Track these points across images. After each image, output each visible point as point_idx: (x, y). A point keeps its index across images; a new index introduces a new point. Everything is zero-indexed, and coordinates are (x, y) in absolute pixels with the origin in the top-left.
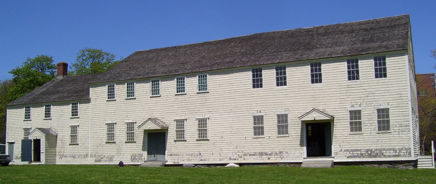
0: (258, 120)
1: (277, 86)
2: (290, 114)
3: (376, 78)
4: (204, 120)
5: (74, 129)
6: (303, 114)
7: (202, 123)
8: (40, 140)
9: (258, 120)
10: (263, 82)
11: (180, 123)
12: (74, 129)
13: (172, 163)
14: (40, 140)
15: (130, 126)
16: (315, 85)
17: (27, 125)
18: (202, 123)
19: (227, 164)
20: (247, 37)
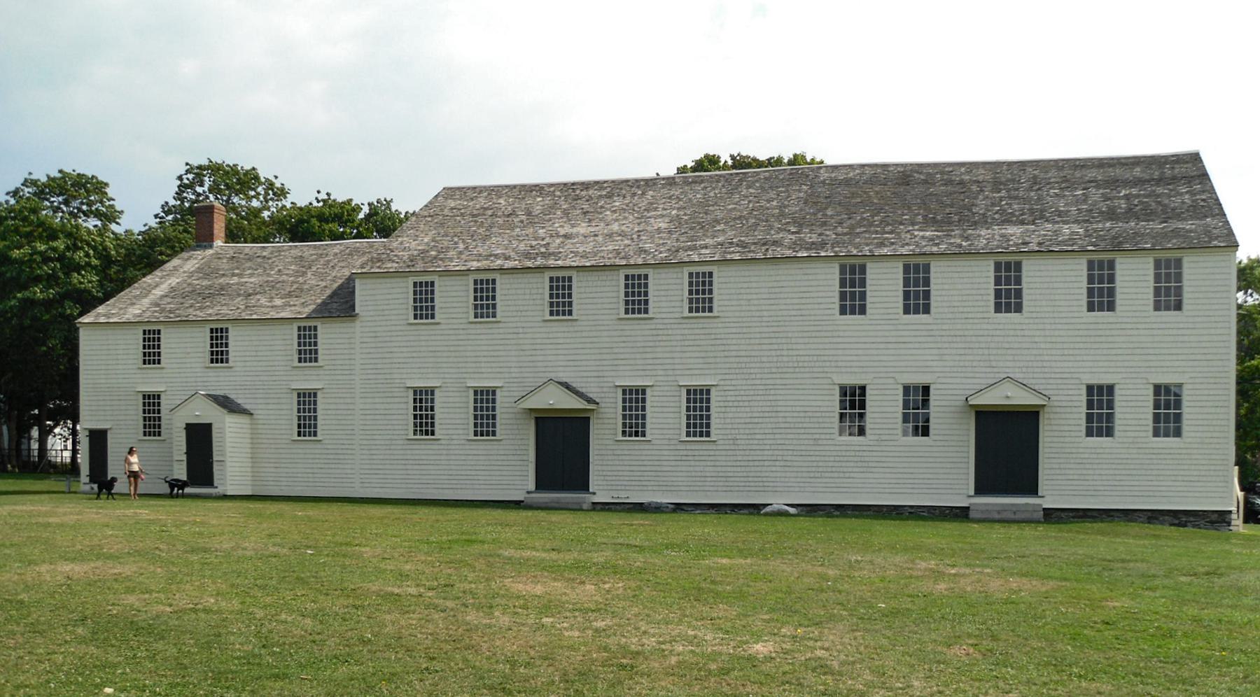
0: (423, 403)
1: (1089, 310)
2: (871, 387)
3: (841, 314)
4: (701, 393)
5: (307, 400)
6: (979, 387)
7: (698, 399)
8: (210, 425)
9: (423, 403)
10: (932, 298)
11: (635, 399)
12: (307, 400)
13: (250, 493)
14: (210, 425)
15: (485, 400)
16: (1097, 315)
17: (151, 381)
18: (698, 399)
19: (766, 505)
20: (868, 171)
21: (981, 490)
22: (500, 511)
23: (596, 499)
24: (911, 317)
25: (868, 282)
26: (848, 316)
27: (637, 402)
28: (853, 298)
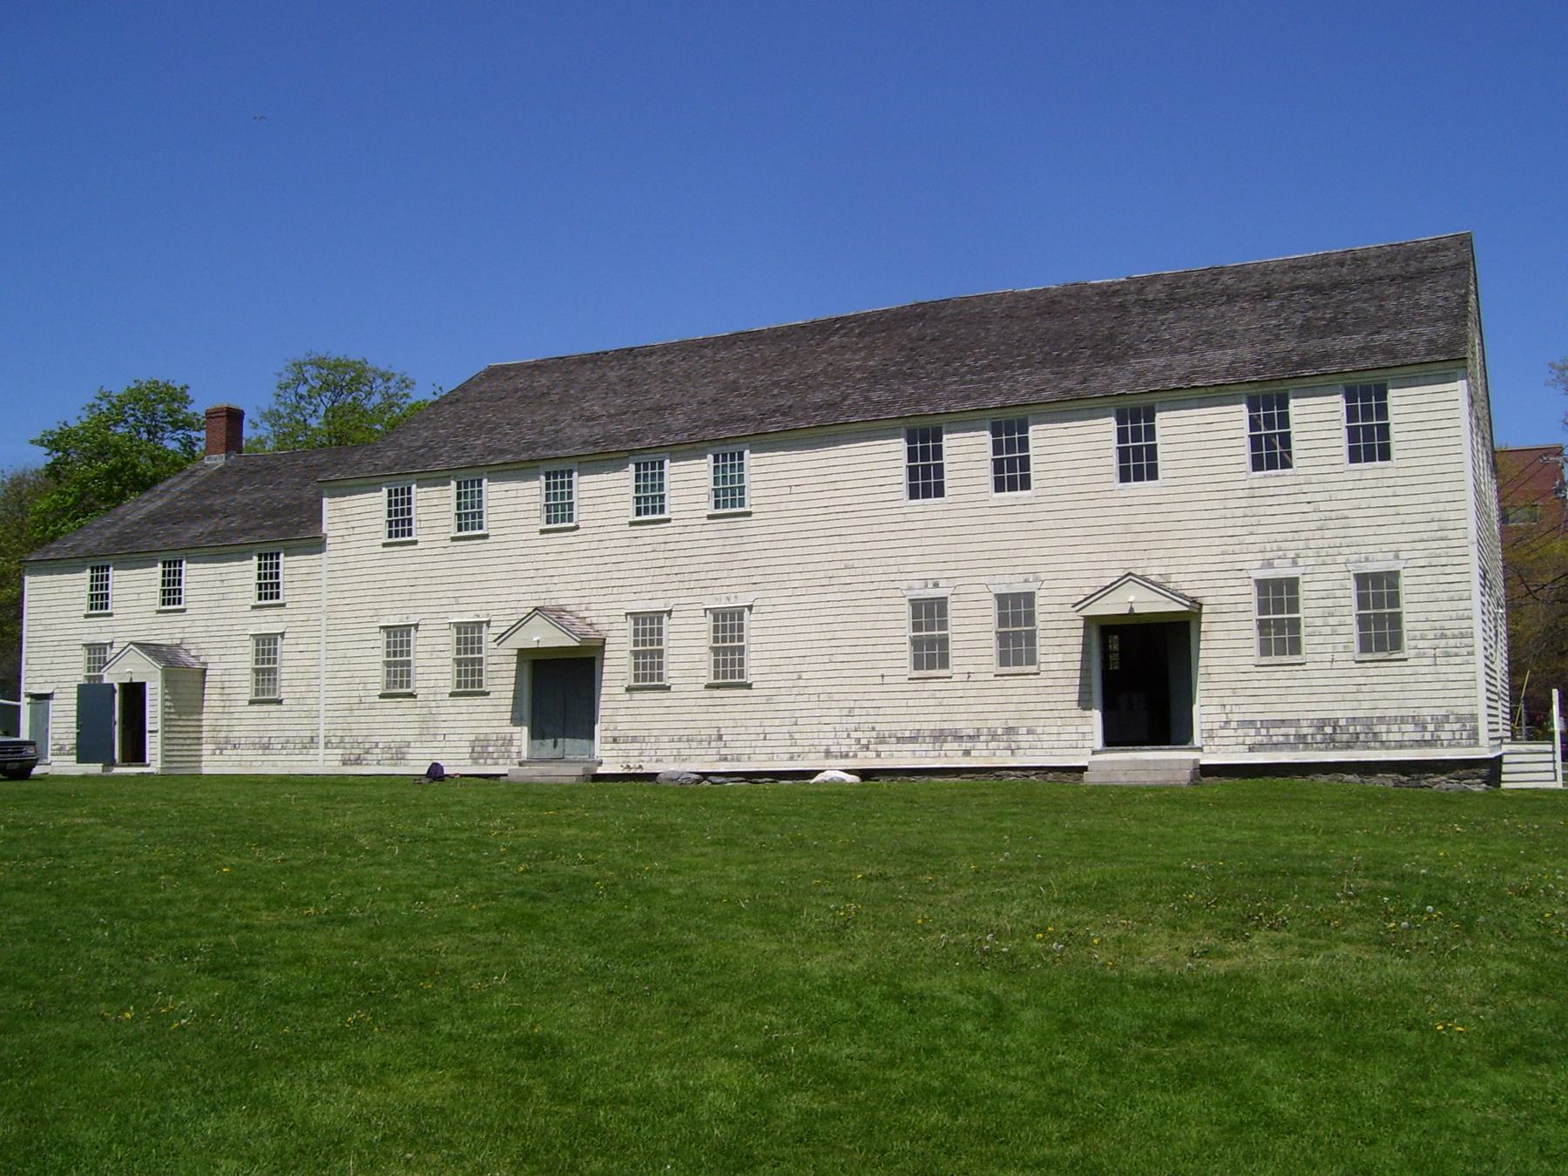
0: (929, 612)
5: (266, 646)
6: (1089, 592)
7: (728, 624)
8: (143, 684)
9: (929, 612)
10: (947, 475)
11: (648, 625)
12: (266, 646)
14: (143, 684)
15: (469, 636)
17: (98, 631)
18: (728, 624)
19: (812, 774)
20: (887, 315)
21: (1113, 738)
22: (1237, 781)
23: (1206, 760)
24: (1006, 495)
25: (1391, 410)
26: (1133, 484)
27: (732, 630)
28: (926, 475)
